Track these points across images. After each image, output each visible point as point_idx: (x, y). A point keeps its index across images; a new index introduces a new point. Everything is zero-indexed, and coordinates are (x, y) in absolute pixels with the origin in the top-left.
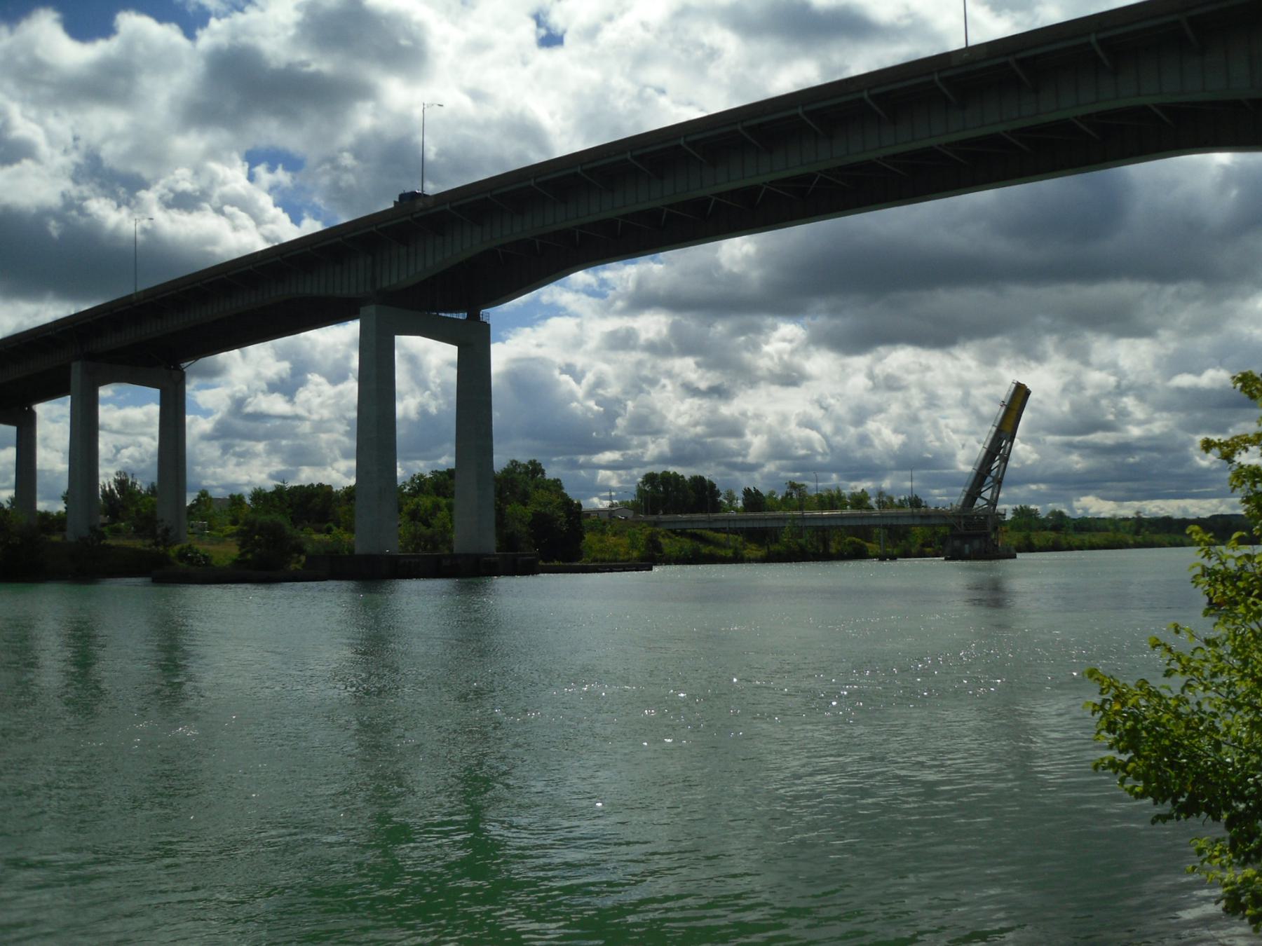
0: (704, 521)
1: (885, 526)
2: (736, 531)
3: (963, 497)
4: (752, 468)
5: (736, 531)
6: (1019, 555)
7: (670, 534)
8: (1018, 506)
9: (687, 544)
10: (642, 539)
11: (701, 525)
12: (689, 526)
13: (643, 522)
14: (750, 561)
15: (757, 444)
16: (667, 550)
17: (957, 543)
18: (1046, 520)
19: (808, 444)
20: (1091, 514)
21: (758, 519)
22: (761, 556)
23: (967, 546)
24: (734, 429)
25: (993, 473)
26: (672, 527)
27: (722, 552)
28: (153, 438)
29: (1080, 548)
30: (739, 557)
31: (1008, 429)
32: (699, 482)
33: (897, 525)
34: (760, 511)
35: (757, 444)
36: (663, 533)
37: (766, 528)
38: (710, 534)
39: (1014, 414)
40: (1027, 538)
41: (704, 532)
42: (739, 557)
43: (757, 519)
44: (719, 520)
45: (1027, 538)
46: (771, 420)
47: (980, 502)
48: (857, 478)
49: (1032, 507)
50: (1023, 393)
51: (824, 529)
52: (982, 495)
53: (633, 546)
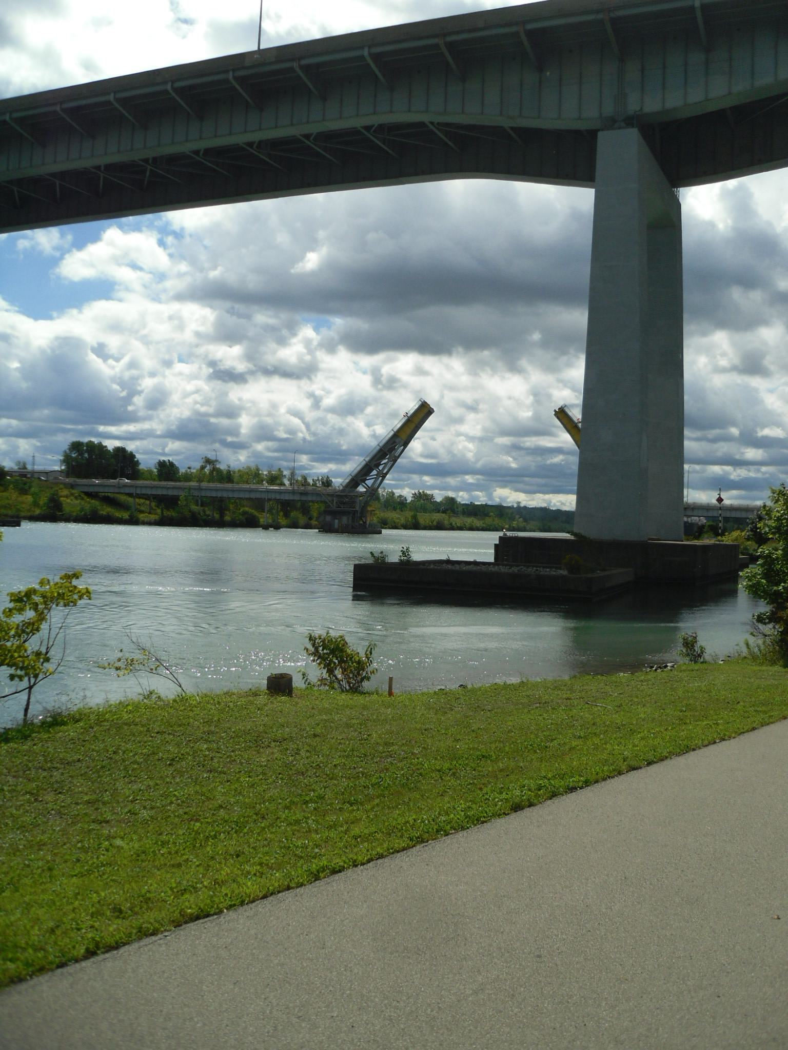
0: (114, 486)
1: (277, 501)
2: (146, 497)
3: (347, 481)
4: (238, 446)
5: (146, 497)
6: (384, 531)
7: (83, 495)
8: (417, 491)
9: (89, 504)
10: (43, 500)
11: (112, 490)
12: (101, 490)
13: (61, 483)
14: (144, 523)
15: (245, 423)
16: (67, 509)
17: (328, 518)
18: (440, 503)
19: (292, 431)
20: (510, 502)
21: (167, 488)
22: (155, 520)
23: (336, 521)
24: (231, 412)
25: (381, 468)
26: (86, 490)
27: (118, 514)
28: (574, 389)
29: (460, 529)
30: (135, 519)
31: (404, 437)
32: (120, 451)
33: (293, 500)
34: (172, 480)
35: (245, 423)
36: (76, 495)
37: (167, 495)
38: (123, 498)
39: (412, 426)
40: (415, 517)
41: (118, 496)
42: (135, 519)
43: (160, 487)
44: (254, 491)
45: (415, 517)
46: (264, 405)
47: (361, 489)
48: (324, 460)
49: (429, 492)
50: (426, 411)
51: (221, 500)
52: (367, 482)
53: (36, 504)
